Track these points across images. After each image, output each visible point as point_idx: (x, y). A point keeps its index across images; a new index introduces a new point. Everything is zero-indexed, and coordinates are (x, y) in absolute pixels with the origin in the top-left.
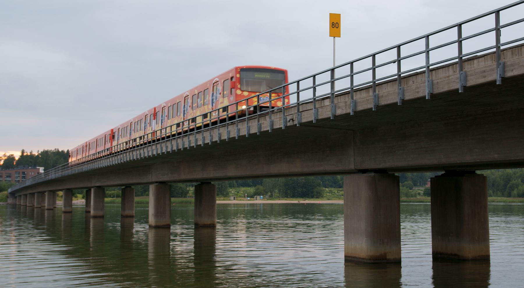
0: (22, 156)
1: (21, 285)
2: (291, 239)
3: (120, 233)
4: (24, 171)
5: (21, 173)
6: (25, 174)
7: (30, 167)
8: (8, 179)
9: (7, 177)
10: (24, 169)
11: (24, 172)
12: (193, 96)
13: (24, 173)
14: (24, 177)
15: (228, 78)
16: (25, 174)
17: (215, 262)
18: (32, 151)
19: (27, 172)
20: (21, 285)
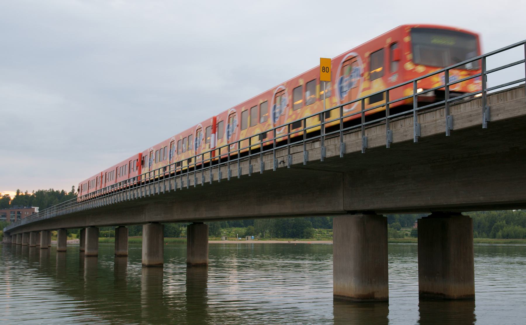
4: (19, 210)
5: (16, 213)
6: (20, 214)
7: (25, 207)
9: (3, 216)
10: (19, 208)
11: (20, 212)
13: (19, 213)
16: (20, 214)
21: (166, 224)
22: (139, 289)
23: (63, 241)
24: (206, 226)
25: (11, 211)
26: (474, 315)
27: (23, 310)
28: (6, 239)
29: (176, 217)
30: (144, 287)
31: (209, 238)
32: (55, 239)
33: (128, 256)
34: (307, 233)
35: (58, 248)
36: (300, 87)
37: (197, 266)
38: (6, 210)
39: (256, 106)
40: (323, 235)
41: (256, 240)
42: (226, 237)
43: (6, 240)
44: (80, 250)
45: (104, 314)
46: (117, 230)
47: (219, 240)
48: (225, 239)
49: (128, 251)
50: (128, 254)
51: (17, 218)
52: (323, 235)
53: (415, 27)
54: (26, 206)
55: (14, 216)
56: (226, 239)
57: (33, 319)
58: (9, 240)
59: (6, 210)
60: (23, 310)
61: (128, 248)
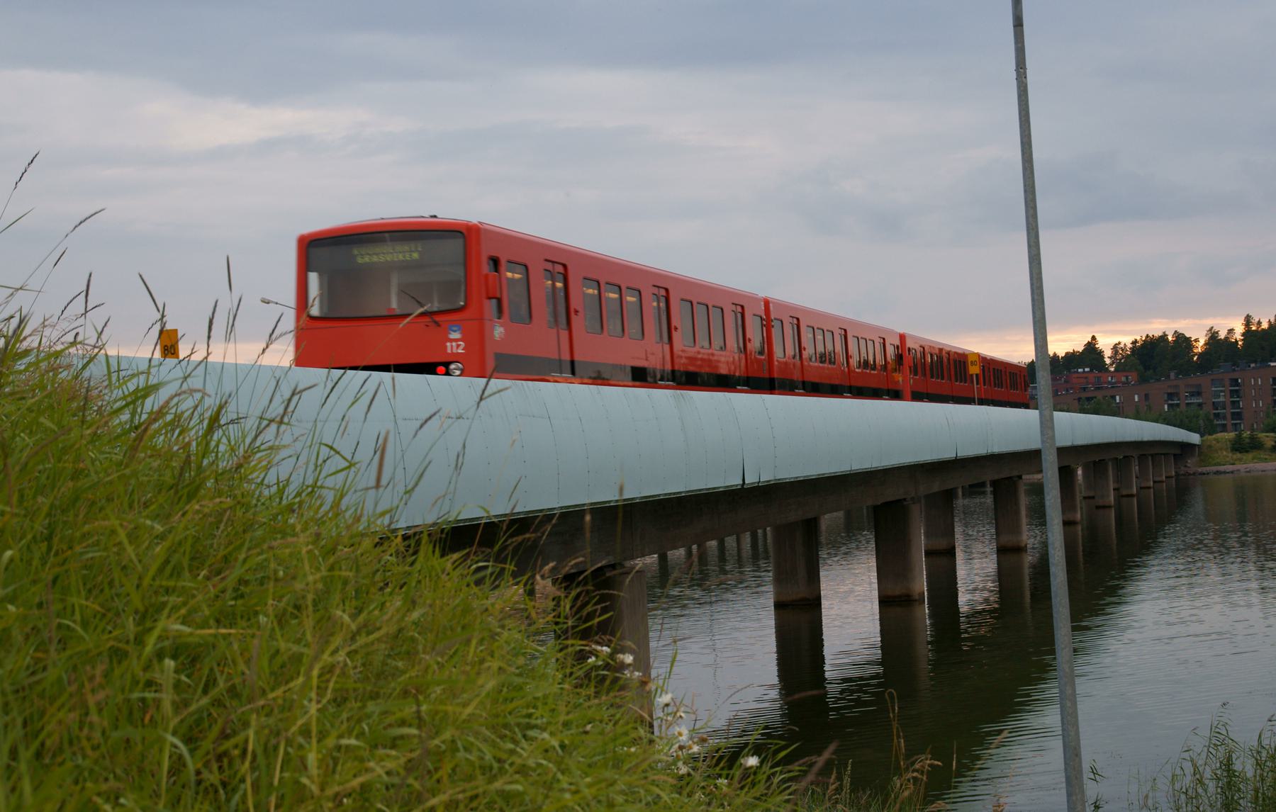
0: (1248, 334)
1: (345, 430)
2: (1045, 734)
3: (956, 519)
4: (1235, 376)
5: (1227, 383)
6: (1238, 385)
7: (1253, 365)
8: (1195, 400)
9: (1192, 395)
10: (1234, 370)
11: (1237, 380)
12: (526, 266)
13: (1234, 382)
14: (1237, 391)
15: (456, 454)
16: (1238, 385)
17: (960, 613)
18: (1094, 338)
19: (1243, 380)
20: (345, 430)
25: (1212, 380)
27: (426, 467)
30: (1024, 520)
32: (1266, 459)
36: (144, 276)
37: (560, 366)
38: (1198, 376)
39: (141, 276)
51: (1231, 397)
53: (470, 224)
54: (1255, 362)
55: (1222, 391)
57: (71, 302)
59: (1198, 376)
60: (426, 467)
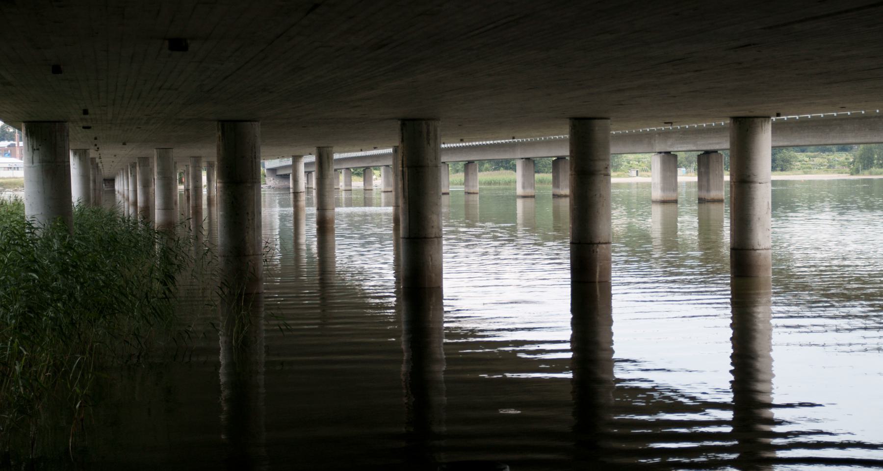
21: (535, 159)
22: (676, 244)
23: (348, 183)
24: (721, 155)
26: (612, 341)
28: (270, 181)
29: (830, 142)
31: (23, 179)
33: (725, 201)
34: (783, 161)
35: (383, 189)
40: (804, 164)
41: (691, 176)
42: (637, 171)
43: (272, 182)
44: (553, 195)
45: (857, 290)
46: (364, 171)
47: (625, 177)
48: (635, 175)
49: (724, 194)
50: (724, 198)
52: (804, 164)
56: (637, 175)
58: (277, 183)
61: (724, 189)
